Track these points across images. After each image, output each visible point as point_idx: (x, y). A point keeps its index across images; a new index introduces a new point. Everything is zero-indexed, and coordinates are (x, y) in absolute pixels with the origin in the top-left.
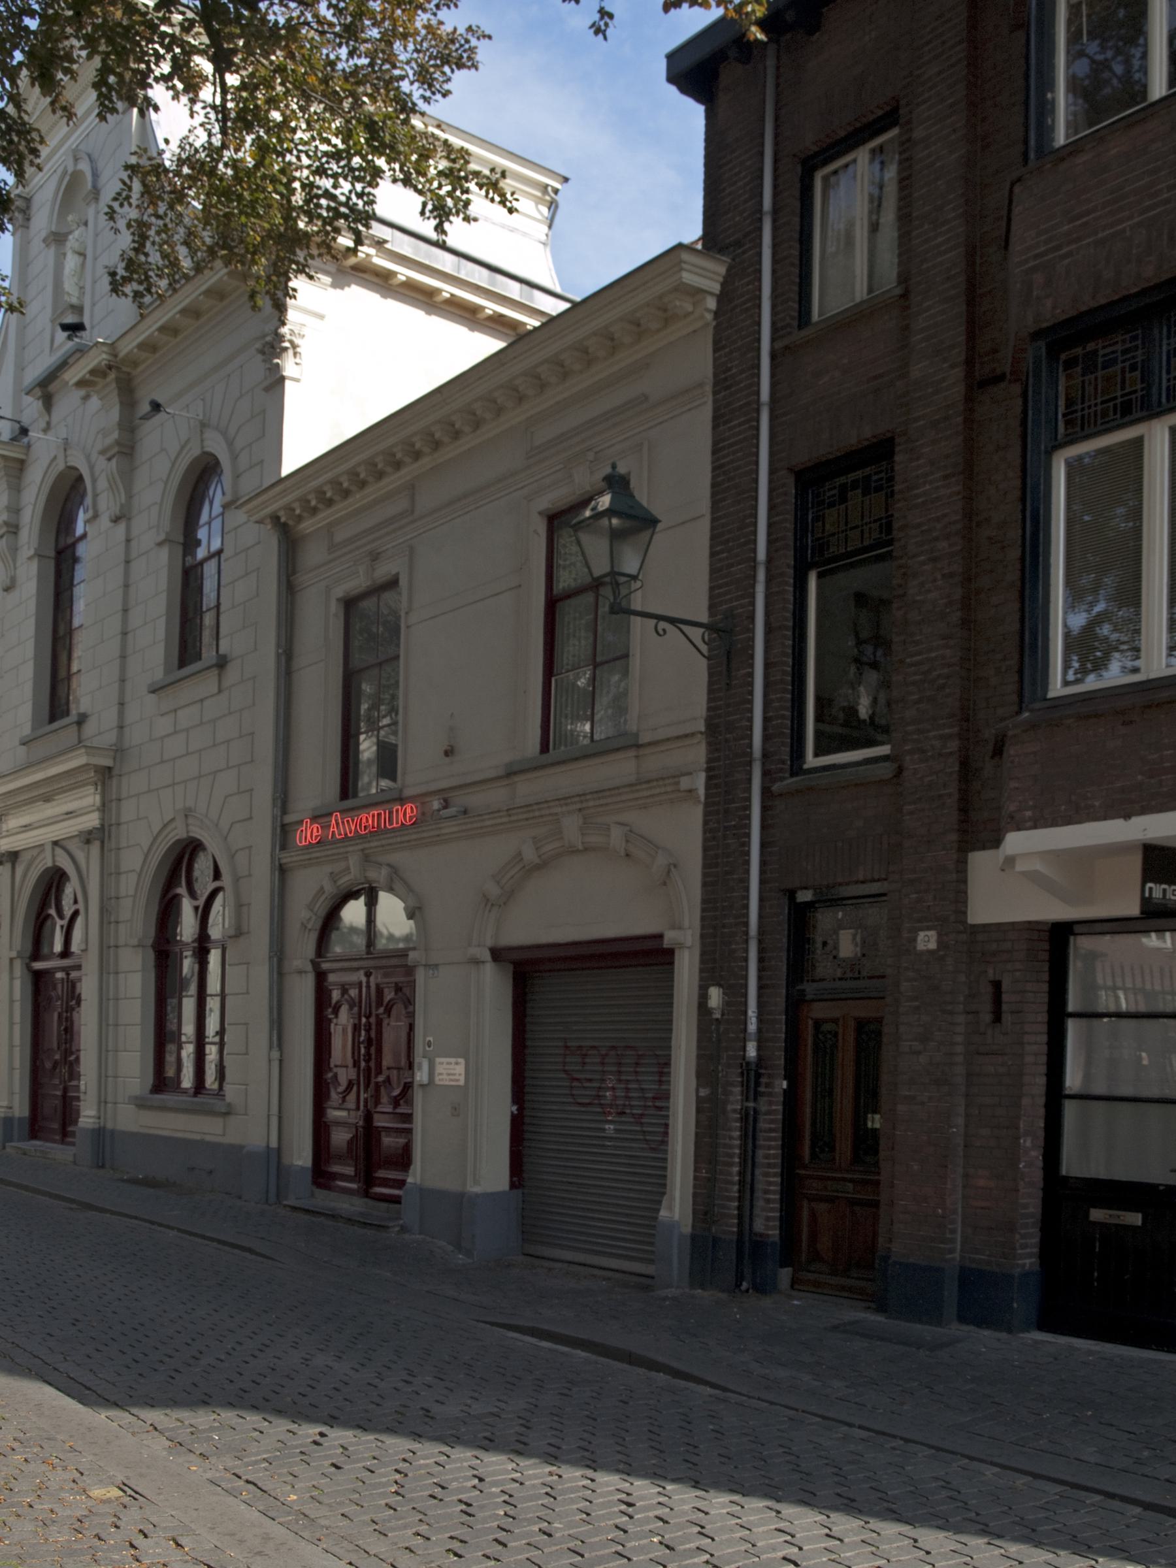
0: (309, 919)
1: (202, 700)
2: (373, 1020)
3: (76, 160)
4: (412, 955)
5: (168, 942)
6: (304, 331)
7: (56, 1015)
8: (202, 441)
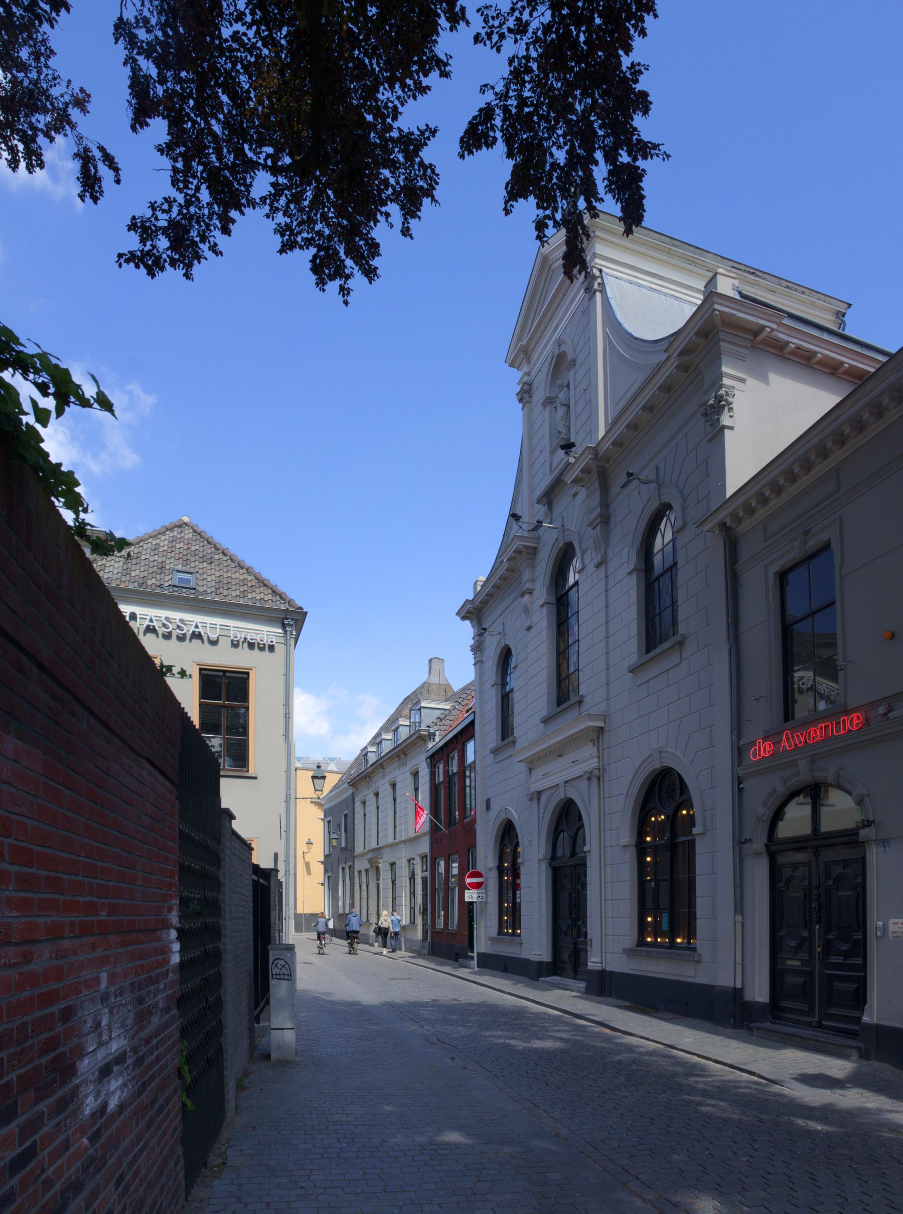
4: (862, 833)
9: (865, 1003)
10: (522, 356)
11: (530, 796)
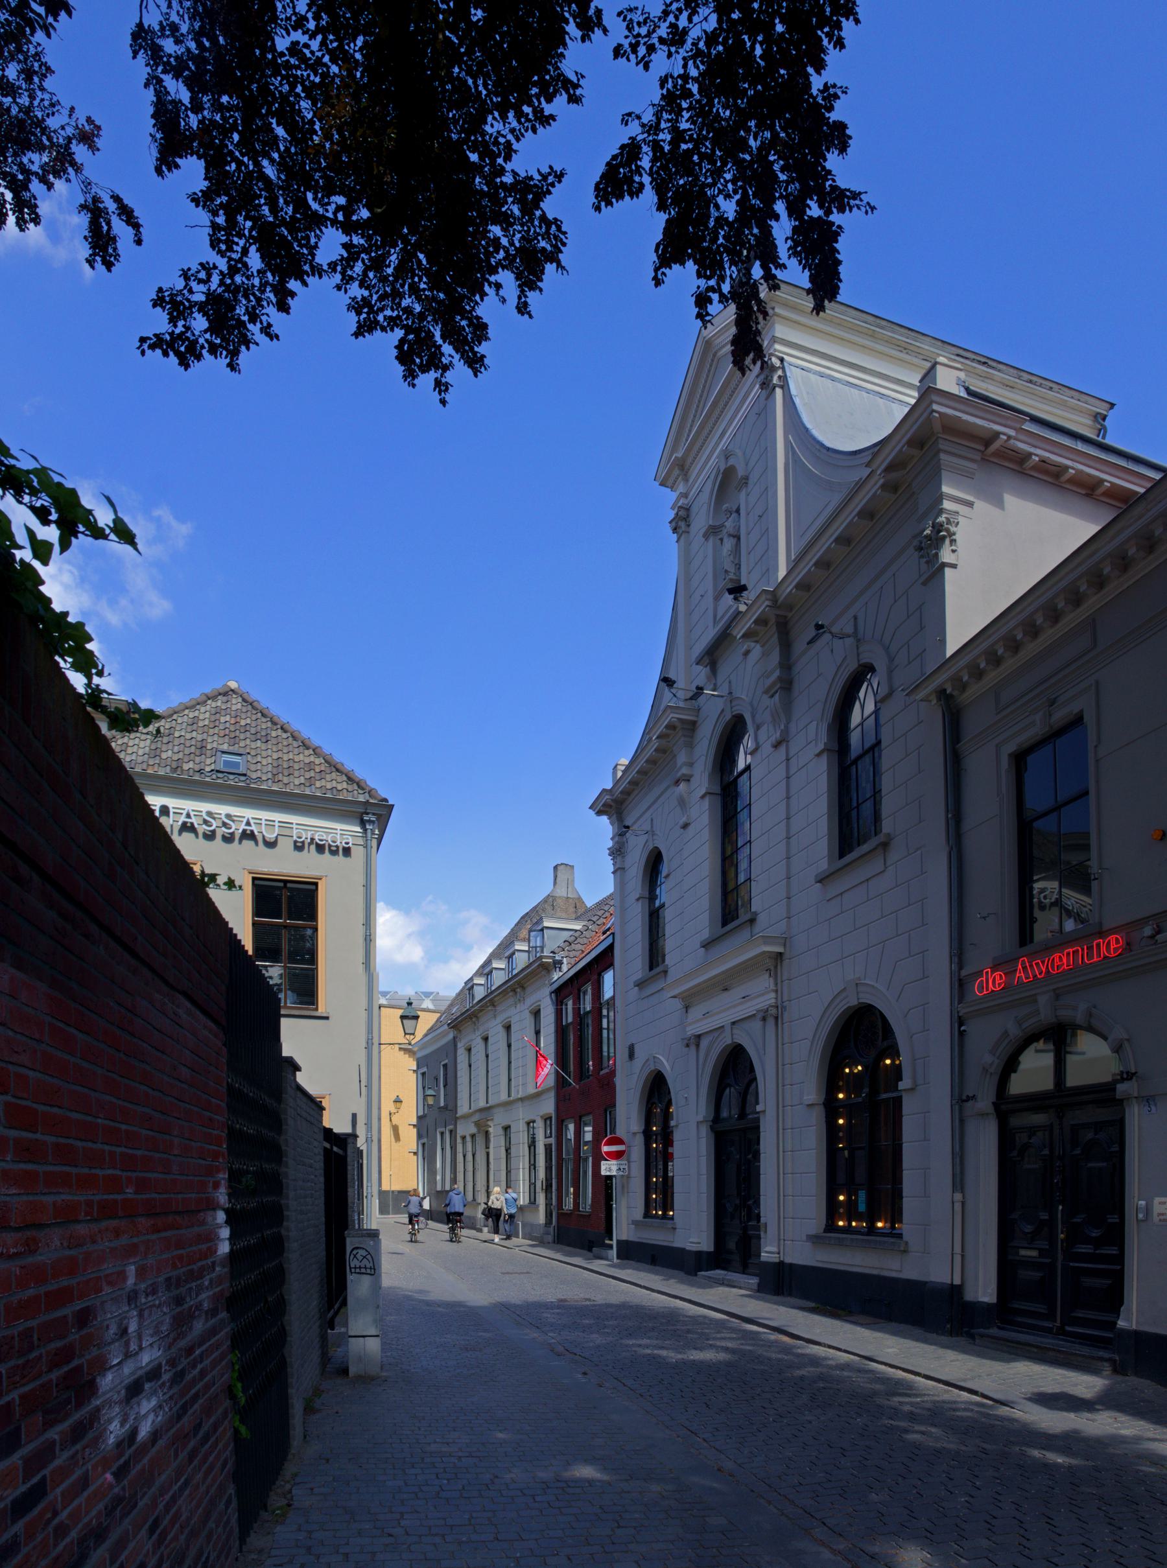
0: (991, 1065)
8: (858, 655)
10: (676, 472)
11: (686, 1041)
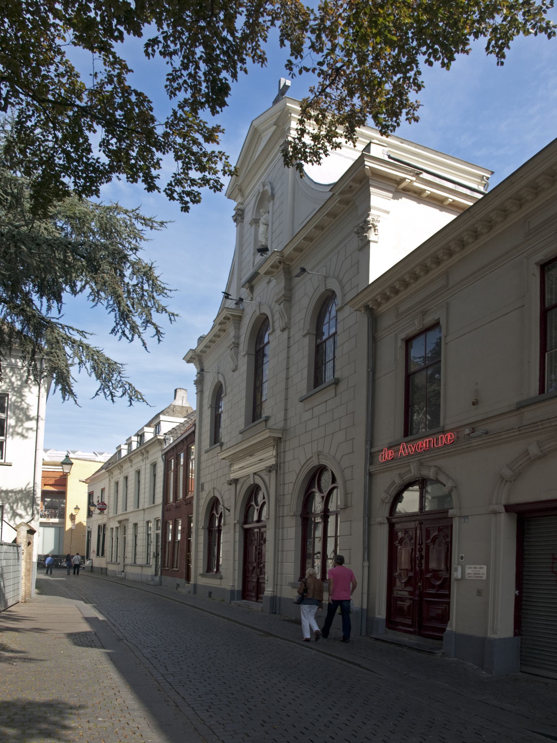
0: (386, 498)
1: (326, 401)
2: (424, 546)
3: (264, 186)
5: (308, 513)
6: (379, 219)
7: (254, 547)
8: (325, 284)
9: (449, 619)
10: (237, 191)
